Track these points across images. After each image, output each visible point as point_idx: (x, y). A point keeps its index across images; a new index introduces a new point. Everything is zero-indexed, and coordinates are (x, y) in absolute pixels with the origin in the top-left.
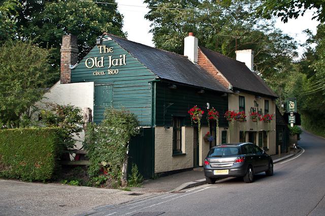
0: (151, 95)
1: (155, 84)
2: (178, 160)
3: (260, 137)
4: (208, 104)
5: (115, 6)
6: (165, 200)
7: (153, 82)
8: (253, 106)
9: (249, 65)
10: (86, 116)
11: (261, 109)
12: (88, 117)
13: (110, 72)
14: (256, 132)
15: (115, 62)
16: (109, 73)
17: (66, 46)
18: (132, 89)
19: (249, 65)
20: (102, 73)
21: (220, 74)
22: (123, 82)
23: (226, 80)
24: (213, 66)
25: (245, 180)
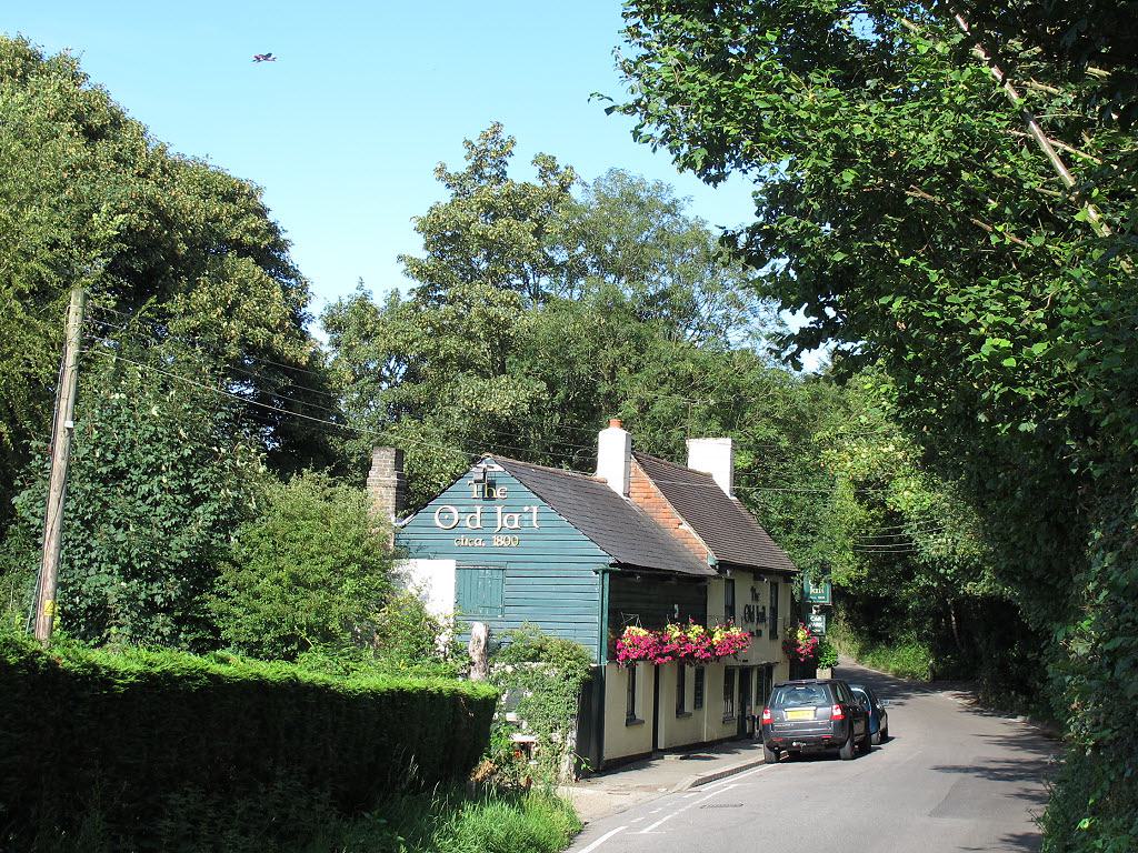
0: (598, 598)
1: (607, 576)
2: (683, 722)
3: (759, 673)
4: (676, 606)
5: (282, 246)
6: (732, 783)
7: (604, 572)
8: (749, 602)
9: (724, 481)
10: (479, 641)
11: (764, 608)
12: (483, 642)
13: (499, 541)
14: (752, 667)
15: (510, 520)
16: (496, 544)
17: (382, 472)
18: (552, 581)
19: (724, 481)
20: (479, 542)
21: (686, 527)
22: (530, 566)
23: (701, 541)
24: (669, 505)
25: (842, 755)
